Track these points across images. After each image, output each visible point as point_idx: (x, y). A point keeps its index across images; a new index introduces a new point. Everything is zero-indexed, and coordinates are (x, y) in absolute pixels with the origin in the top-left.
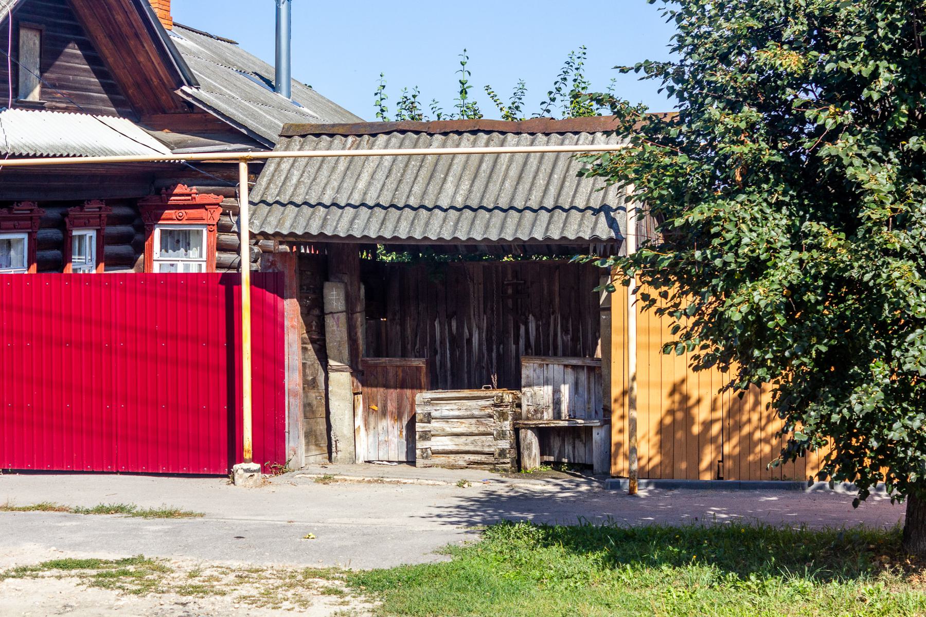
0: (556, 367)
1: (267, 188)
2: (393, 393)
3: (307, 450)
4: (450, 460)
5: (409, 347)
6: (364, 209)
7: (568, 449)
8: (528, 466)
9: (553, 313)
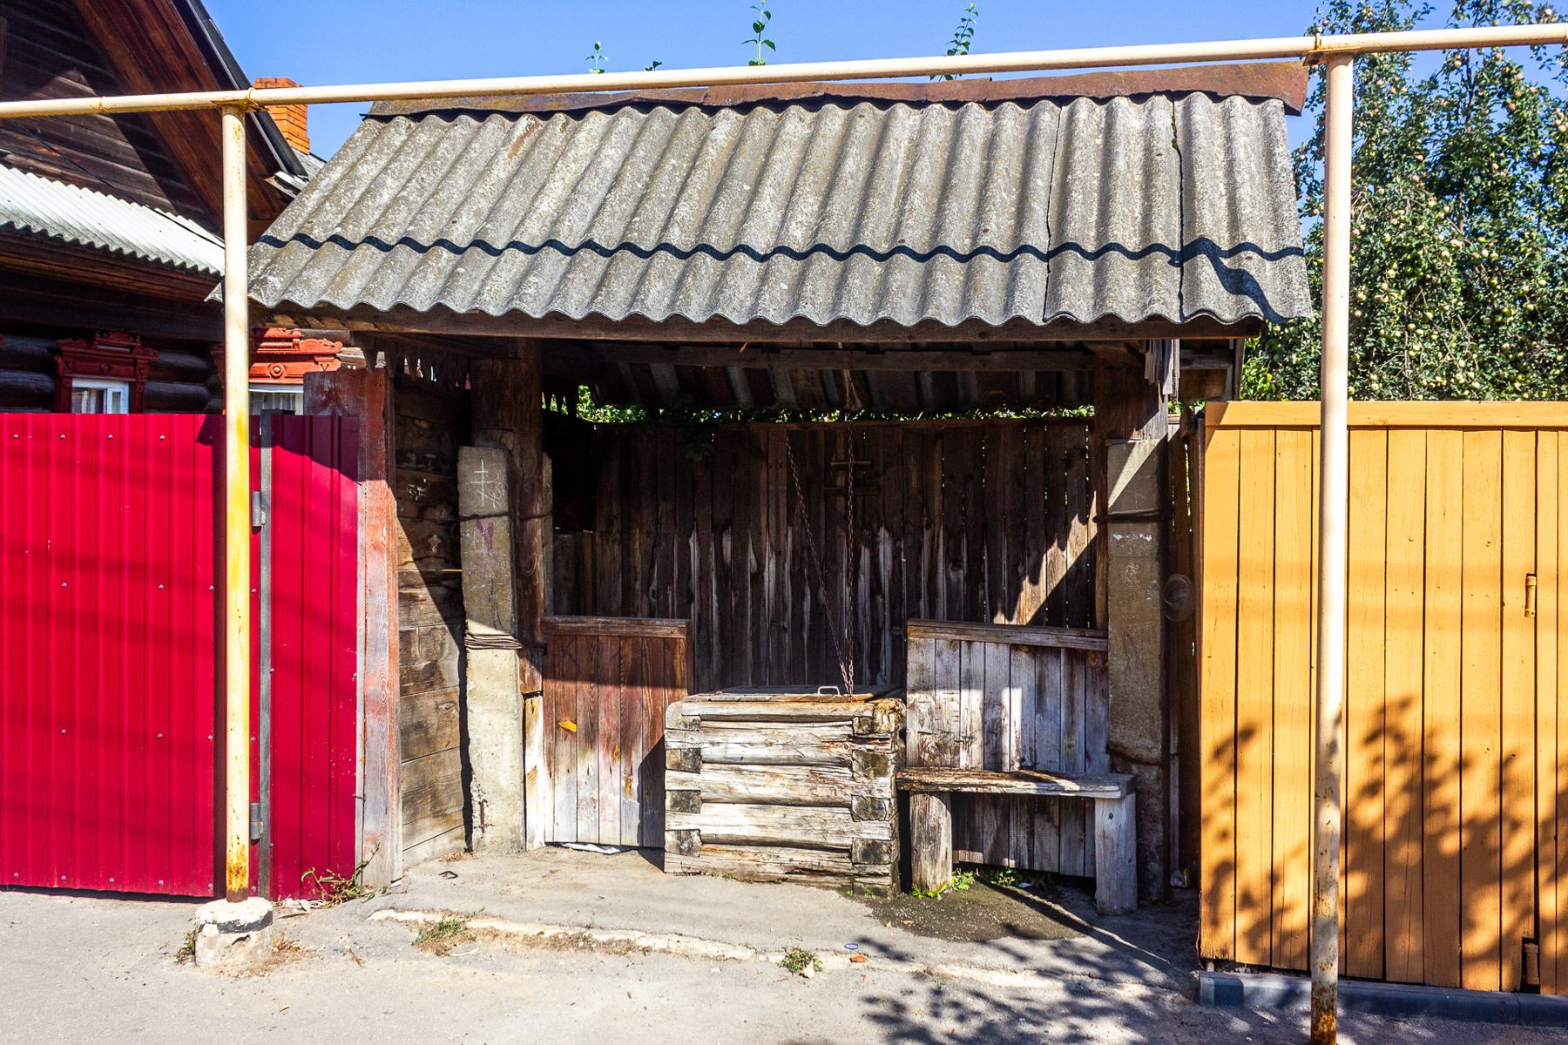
0: (991, 648)
1: (319, 208)
2: (612, 695)
3: (411, 833)
4: (745, 861)
5: (638, 585)
6: (554, 254)
7: (1017, 837)
8: (930, 880)
9: (928, 526)
